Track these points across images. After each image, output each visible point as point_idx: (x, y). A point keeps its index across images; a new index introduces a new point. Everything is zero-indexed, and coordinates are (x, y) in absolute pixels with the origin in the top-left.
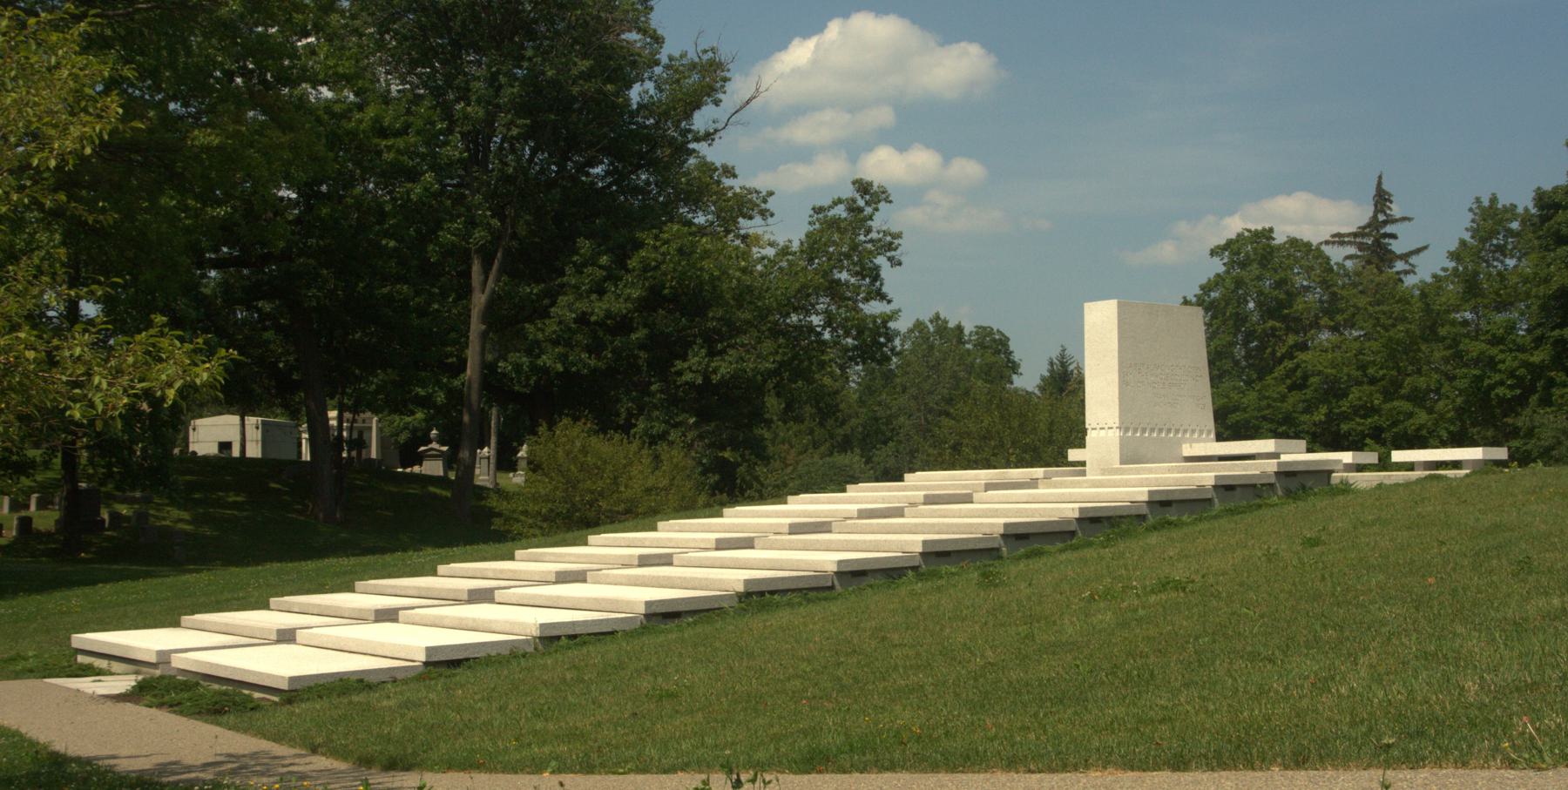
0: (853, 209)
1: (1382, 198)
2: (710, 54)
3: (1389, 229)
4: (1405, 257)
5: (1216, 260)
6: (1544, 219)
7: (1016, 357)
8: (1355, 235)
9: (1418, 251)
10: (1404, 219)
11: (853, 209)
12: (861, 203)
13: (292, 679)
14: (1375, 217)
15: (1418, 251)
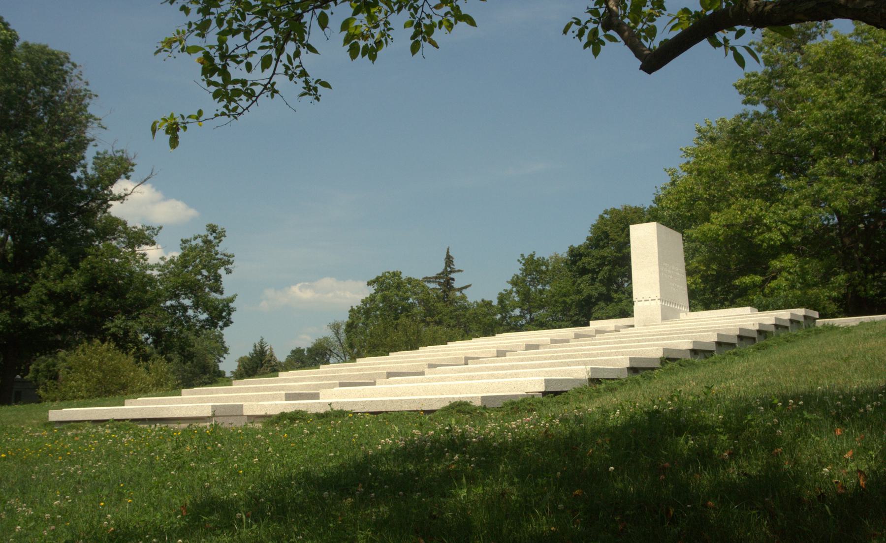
0: (206, 242)
1: (449, 260)
2: (121, 153)
3: (452, 276)
4: (460, 290)
5: (371, 287)
6: (574, 262)
7: (226, 345)
8: (436, 278)
9: (466, 287)
10: (459, 271)
11: (206, 242)
12: (211, 238)
13: (484, 399)
14: (446, 269)
15: (466, 287)
